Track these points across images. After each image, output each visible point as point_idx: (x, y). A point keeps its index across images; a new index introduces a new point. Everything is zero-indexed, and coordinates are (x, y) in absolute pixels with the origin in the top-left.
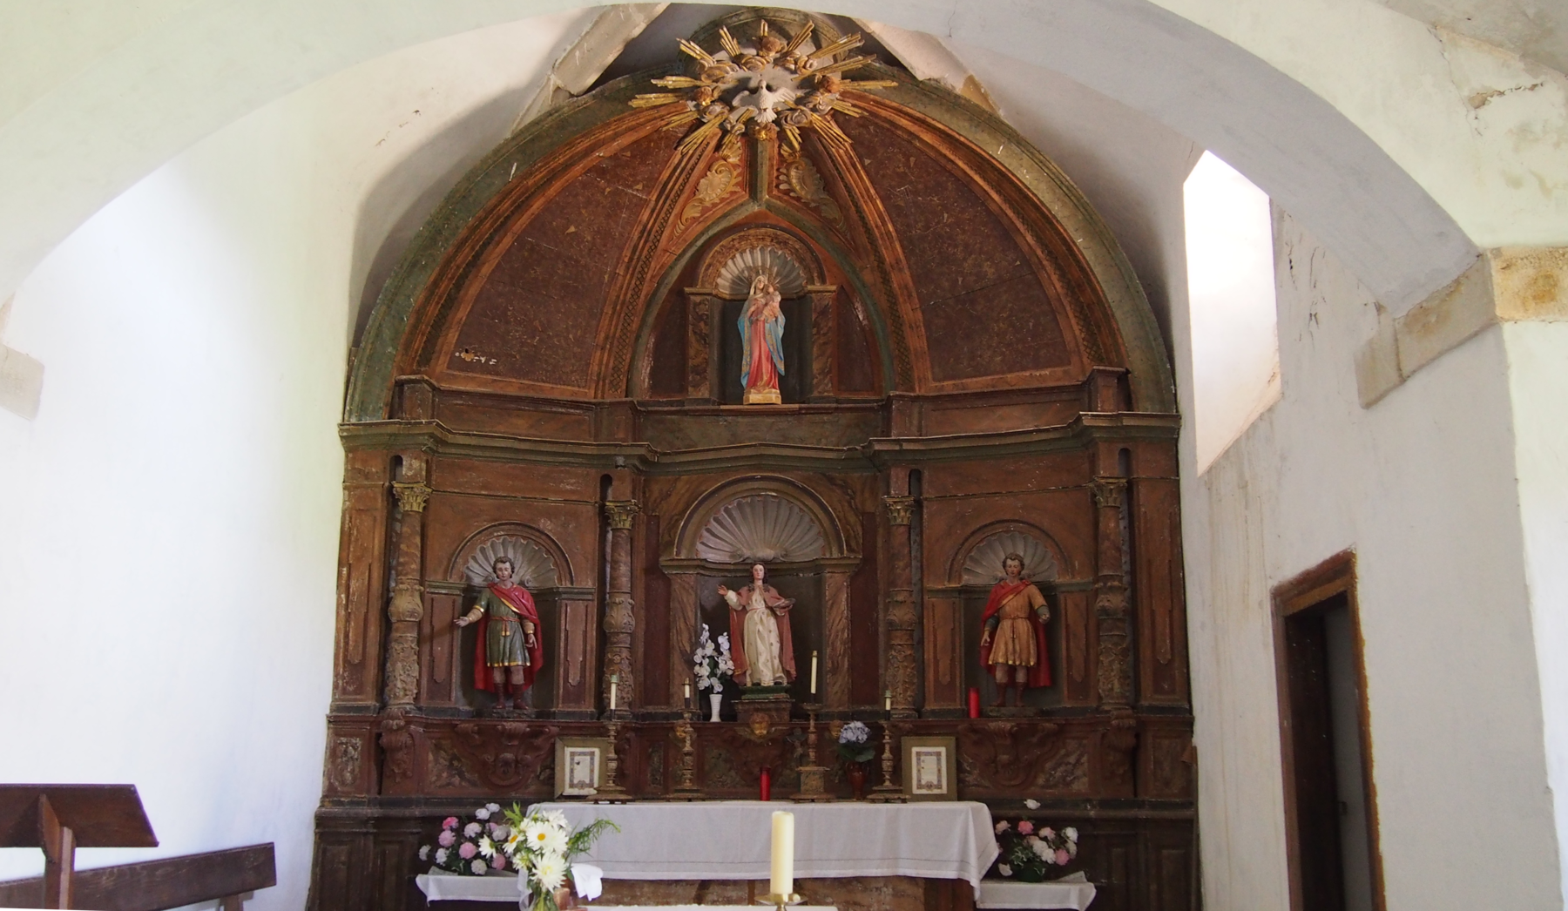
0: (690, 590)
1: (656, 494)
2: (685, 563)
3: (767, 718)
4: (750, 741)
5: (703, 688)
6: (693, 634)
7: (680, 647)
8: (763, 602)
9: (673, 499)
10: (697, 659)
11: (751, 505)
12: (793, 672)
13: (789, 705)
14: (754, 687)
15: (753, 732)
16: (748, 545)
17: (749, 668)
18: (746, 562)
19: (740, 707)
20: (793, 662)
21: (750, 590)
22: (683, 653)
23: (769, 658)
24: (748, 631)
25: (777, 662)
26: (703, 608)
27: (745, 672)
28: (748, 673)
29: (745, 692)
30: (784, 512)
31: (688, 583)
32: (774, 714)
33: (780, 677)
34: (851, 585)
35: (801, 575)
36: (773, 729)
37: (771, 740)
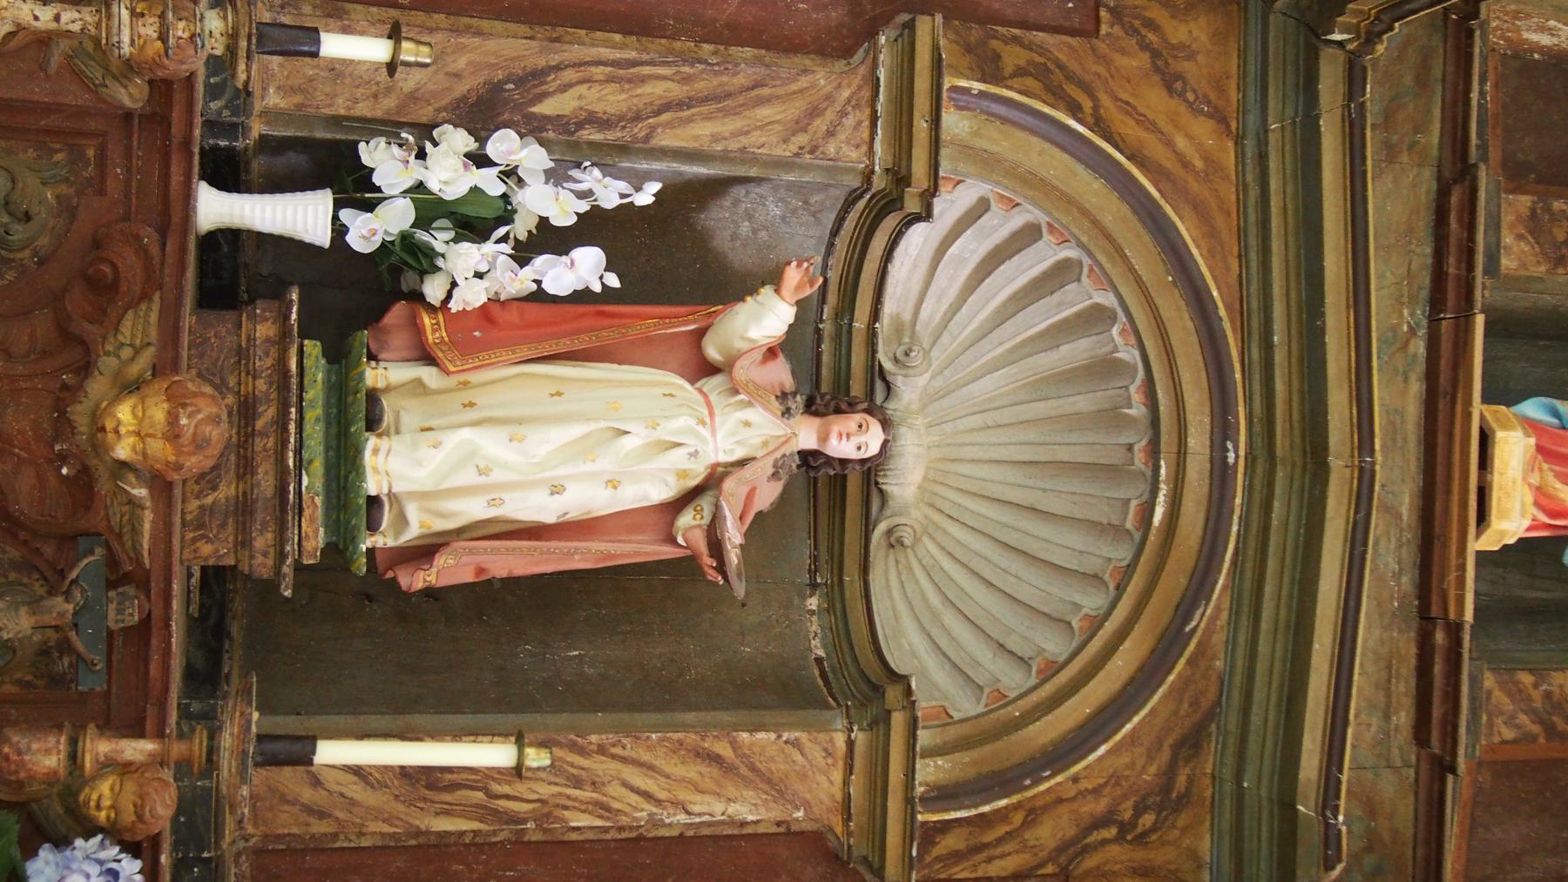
0: (802, 139)
1: (1179, 32)
2: (921, 126)
3: (195, 463)
4: (85, 368)
5: (366, 160)
6: (611, 136)
7: (558, 68)
8: (739, 454)
9: (1154, 100)
10: (503, 145)
11: (1112, 417)
12: (415, 580)
13: (262, 566)
14: (362, 396)
15: (131, 387)
16: (940, 395)
17: (452, 381)
18: (879, 385)
19: (265, 330)
20: (468, 577)
21: (783, 396)
22: (534, 80)
23: (497, 476)
24: (621, 383)
25: (475, 510)
26: (714, 188)
27: (428, 359)
28: (427, 374)
29: (339, 356)
30: (1067, 545)
31: (831, 133)
32: (226, 491)
33: (402, 521)
34: (788, 835)
35: (813, 603)
36: (141, 492)
37: (84, 483)
